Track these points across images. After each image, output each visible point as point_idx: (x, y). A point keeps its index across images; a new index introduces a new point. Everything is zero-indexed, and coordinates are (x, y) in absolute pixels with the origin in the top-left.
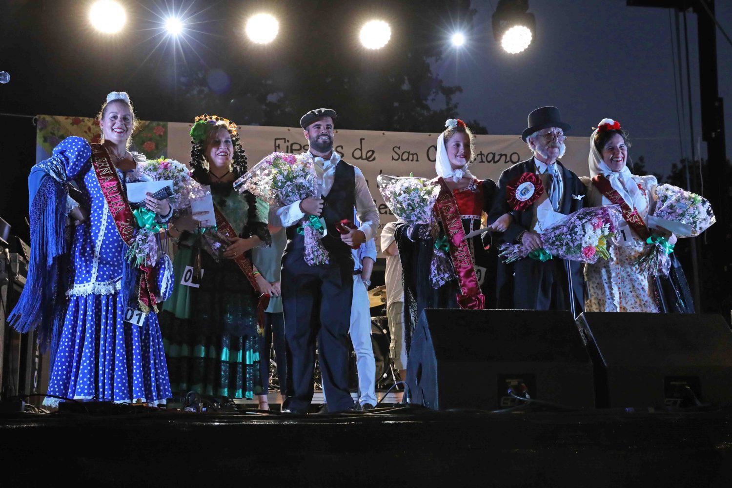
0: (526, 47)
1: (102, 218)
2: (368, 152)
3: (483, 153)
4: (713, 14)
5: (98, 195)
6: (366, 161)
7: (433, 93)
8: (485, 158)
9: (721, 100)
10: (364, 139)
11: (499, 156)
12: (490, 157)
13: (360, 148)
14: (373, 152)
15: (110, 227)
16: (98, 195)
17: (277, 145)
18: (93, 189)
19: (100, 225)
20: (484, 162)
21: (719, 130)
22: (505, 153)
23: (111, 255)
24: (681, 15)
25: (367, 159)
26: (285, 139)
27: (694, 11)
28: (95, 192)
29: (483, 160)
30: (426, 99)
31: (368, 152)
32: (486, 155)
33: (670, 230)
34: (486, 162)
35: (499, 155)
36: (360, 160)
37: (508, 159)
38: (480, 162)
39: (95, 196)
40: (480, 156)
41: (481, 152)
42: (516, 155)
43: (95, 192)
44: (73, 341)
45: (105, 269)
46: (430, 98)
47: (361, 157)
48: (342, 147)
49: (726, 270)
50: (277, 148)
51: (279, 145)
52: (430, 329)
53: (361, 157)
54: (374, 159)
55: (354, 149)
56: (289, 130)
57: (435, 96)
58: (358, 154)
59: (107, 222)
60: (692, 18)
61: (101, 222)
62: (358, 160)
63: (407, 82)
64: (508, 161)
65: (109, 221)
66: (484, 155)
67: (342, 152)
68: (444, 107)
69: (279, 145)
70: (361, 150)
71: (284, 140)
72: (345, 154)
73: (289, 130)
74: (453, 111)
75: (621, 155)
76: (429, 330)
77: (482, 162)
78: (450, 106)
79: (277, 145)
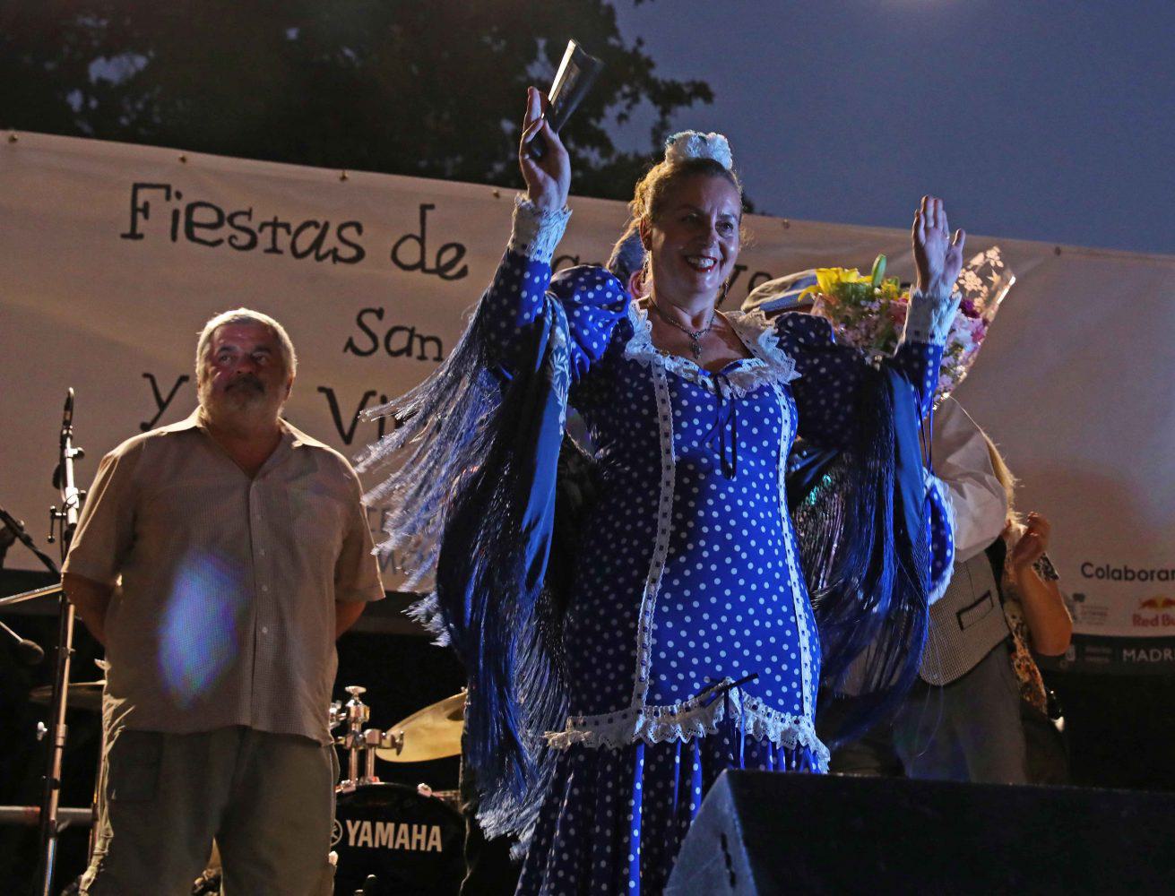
1: (656, 509)
2: (445, 248)
5: (644, 443)
6: (436, 277)
7: (625, 96)
8: (290, 238)
10: (432, 207)
13: (418, 234)
14: (461, 251)
15: (684, 535)
16: (644, 443)
17: (140, 205)
18: (628, 425)
19: (654, 533)
20: (280, 252)
22: (357, 220)
23: (688, 619)
25: (441, 271)
26: (168, 188)
28: (633, 433)
29: (279, 246)
31: (445, 248)
32: (293, 229)
36: (418, 272)
38: (124, 236)
39: (634, 446)
40: (268, 230)
43: (633, 433)
45: (674, 664)
46: (611, 112)
47: (421, 265)
50: (140, 216)
51: (146, 204)
52: (747, 844)
53: (421, 265)
54: (463, 273)
55: (398, 238)
56: (13, 140)
57: (629, 107)
58: (410, 253)
59: (674, 521)
61: (654, 524)
65: (679, 516)
69: (146, 204)
70: (421, 240)
71: (163, 192)
73: (787, 226)
75: (714, 252)
76: (744, 849)
77: (274, 250)
79: (140, 205)
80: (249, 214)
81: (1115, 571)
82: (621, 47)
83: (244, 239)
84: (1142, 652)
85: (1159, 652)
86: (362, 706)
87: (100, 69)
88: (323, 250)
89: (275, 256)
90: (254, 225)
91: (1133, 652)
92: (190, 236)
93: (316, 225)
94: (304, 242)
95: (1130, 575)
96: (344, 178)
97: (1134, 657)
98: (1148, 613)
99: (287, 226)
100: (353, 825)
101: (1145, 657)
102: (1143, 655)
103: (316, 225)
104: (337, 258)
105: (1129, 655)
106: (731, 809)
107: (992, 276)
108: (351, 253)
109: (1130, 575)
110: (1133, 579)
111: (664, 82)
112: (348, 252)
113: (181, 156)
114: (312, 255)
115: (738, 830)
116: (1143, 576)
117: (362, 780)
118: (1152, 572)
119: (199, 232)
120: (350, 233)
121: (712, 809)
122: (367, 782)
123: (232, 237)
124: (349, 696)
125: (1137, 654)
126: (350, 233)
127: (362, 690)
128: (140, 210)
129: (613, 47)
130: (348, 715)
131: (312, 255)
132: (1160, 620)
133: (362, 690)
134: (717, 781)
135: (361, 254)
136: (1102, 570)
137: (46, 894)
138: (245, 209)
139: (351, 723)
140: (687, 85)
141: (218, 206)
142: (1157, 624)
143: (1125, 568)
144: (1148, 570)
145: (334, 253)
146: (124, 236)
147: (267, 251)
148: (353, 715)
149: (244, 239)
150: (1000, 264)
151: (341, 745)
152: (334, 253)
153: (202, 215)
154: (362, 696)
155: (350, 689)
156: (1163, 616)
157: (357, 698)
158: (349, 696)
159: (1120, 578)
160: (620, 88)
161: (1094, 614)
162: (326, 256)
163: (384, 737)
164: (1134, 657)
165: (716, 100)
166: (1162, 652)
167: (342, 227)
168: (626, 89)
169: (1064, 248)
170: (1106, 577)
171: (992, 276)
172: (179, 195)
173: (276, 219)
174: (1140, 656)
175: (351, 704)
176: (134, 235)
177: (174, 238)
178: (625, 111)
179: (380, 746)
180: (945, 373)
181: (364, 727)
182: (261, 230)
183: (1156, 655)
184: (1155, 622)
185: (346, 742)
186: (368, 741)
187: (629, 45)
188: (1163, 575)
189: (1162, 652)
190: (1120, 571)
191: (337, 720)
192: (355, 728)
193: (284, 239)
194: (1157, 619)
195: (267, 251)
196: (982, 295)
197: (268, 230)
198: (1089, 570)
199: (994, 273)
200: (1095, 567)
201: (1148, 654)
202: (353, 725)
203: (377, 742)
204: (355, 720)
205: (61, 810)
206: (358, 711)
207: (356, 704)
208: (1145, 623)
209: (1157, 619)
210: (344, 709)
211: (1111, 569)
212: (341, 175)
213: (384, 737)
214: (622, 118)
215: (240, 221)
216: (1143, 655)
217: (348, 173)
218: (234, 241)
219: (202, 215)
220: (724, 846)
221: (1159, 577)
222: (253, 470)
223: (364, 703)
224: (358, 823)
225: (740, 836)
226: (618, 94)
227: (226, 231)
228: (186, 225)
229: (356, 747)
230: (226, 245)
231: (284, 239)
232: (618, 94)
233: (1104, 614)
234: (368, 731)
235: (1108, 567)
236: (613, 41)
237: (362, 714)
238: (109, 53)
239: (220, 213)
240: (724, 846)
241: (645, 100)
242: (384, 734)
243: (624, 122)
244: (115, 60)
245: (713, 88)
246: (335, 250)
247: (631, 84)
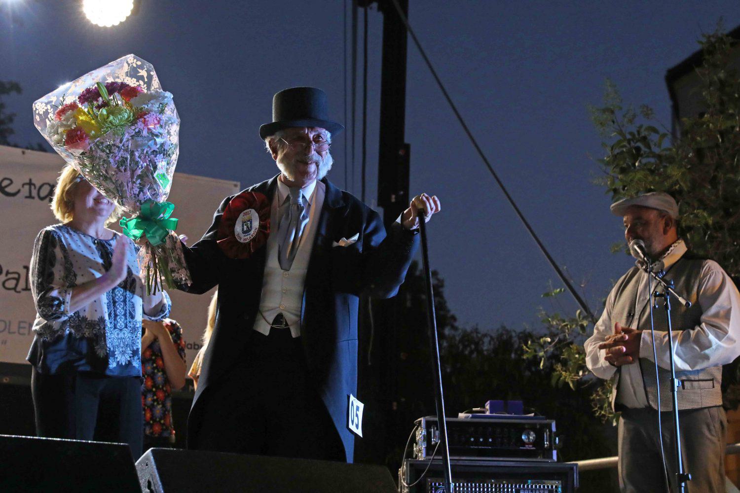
0: (123, 19)
2: (5, 179)
3: (33, 182)
4: (406, 12)
9: (407, 147)
12: (189, 346)
20: (33, 198)
21: (402, 193)
24: (361, 10)
27: (380, 8)
32: (38, 186)
34: (36, 198)
38: (27, 197)
40: (27, 187)
41: (30, 180)
47: (15, 289)
49: (395, 408)
60: (376, 18)
62: (8, 292)
66: (34, 185)
77: (30, 196)
107: (108, 80)
137: (683, 492)
143: (194, 343)
150: (139, 63)
159: (191, 348)
171: (108, 80)
190: (191, 345)
196: (49, 111)
199: (140, 70)
205: (37, 431)
211: (187, 343)
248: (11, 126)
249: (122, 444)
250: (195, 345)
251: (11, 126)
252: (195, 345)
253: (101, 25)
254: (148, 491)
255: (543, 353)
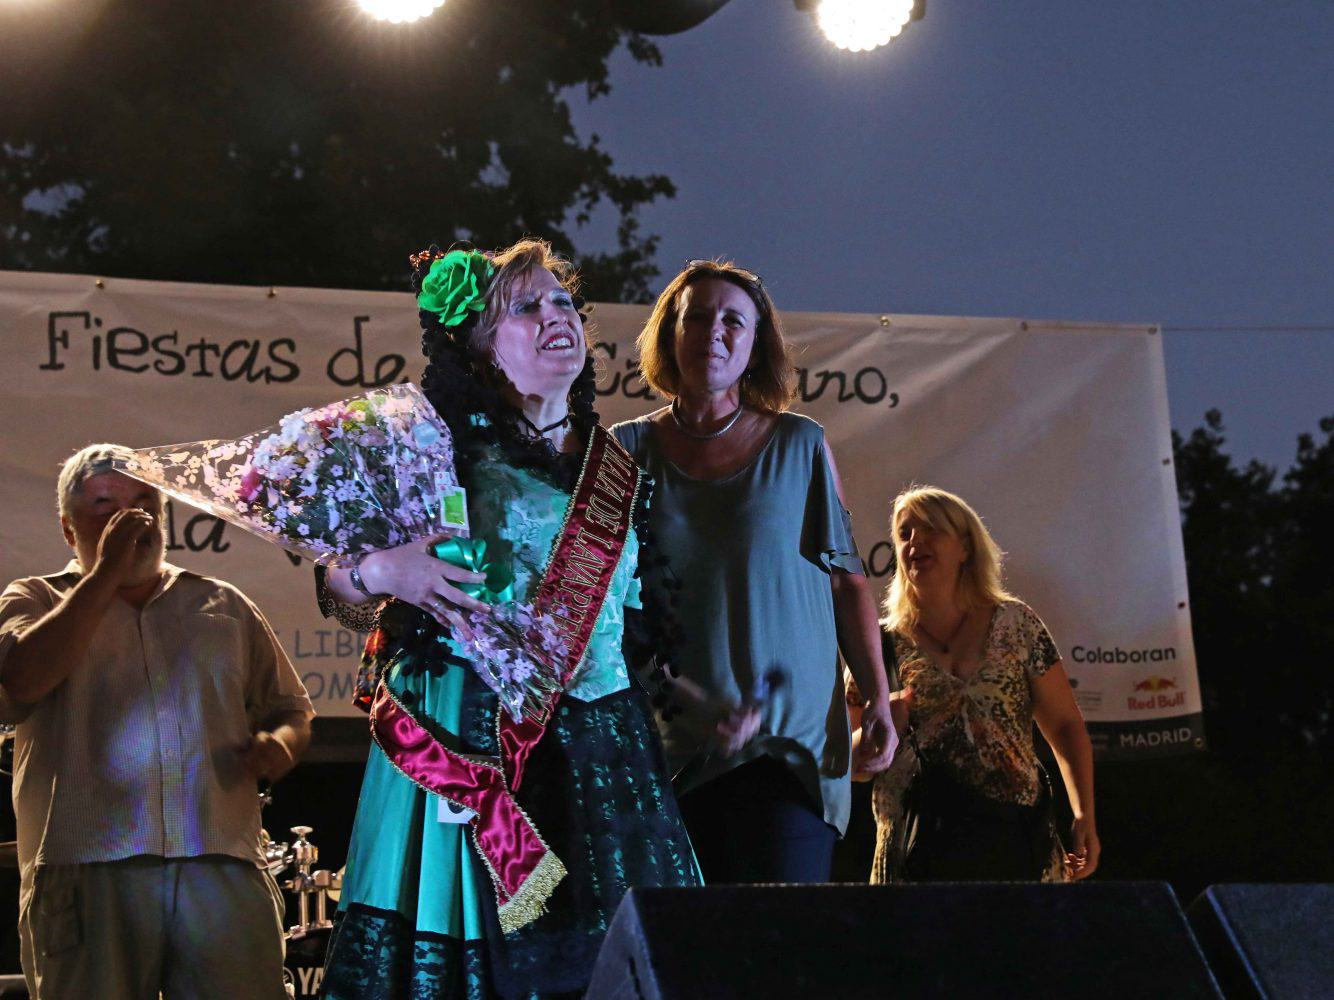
0: (896, 31)
7: (584, 196)
8: (218, 361)
10: (366, 319)
11: (820, 379)
13: (354, 347)
17: (58, 334)
20: (209, 375)
26: (86, 315)
30: (559, 218)
32: (222, 349)
33: (357, 708)
35: (818, 375)
37: (850, 388)
38: (43, 367)
40: (196, 353)
42: (874, 375)
44: (816, 592)
46: (571, 213)
48: (292, 346)
50: (59, 345)
51: (65, 334)
52: (655, 965)
55: (335, 351)
57: (588, 207)
63: (496, 160)
64: (850, 396)
67: (293, 361)
68: (614, 250)
70: (358, 354)
71: (82, 320)
72: (303, 371)
74: (642, 264)
77: (203, 372)
78: (633, 245)
79: (58, 334)
80: (174, 337)
81: (1106, 653)
82: (576, 146)
83: (170, 363)
84: (1140, 736)
85: (1157, 735)
86: (309, 846)
87: (37, 201)
88: (255, 370)
89: (204, 379)
90: (181, 349)
91: (1131, 737)
92: (114, 362)
93: (245, 344)
94: (233, 365)
95: (1122, 657)
96: (271, 295)
97: (1132, 743)
98: (1144, 696)
99: (215, 348)
100: (305, 972)
101: (1143, 741)
102: (1141, 739)
103: (245, 344)
104: (270, 378)
105: (1127, 740)
106: (637, 929)
108: (284, 371)
109: (1122, 657)
110: (1125, 661)
111: (623, 179)
112: (281, 371)
113: (98, 282)
114: (245, 375)
115: (645, 951)
116: (1135, 657)
117: (313, 925)
118: (1145, 653)
119: (122, 359)
120: (282, 351)
121: (621, 931)
122: (318, 926)
123: (157, 363)
124: (294, 838)
125: (1135, 740)
126: (282, 351)
127: (308, 829)
128: (57, 339)
129: (568, 146)
130: (295, 857)
131: (244, 376)
132: (1156, 701)
133: (308, 829)
134: (623, 902)
135: (295, 372)
136: (1093, 653)
138: (170, 332)
139: (299, 866)
140: (648, 180)
141: (142, 331)
142: (1153, 707)
143: (1117, 649)
144: (1162, 647)
145: (267, 373)
146: (43, 367)
147: (196, 374)
148: (299, 856)
149: (170, 363)
151: (290, 889)
152: (267, 373)
153: (121, 341)
154: (309, 837)
155: (295, 829)
156: (1159, 698)
157: (304, 839)
158: (294, 838)
159: (1112, 661)
160: (577, 188)
161: (1089, 699)
162: (258, 376)
163: (335, 878)
164: (1132, 743)
165: (678, 194)
166: (1161, 734)
167: (273, 345)
168: (585, 188)
169: (1031, 323)
170: (1097, 659)
172: (98, 322)
173: (203, 340)
174: (1138, 741)
175: (297, 845)
176: (53, 365)
177: (97, 365)
178: (584, 211)
179: (330, 887)
180: (373, 418)
181: (313, 868)
182: (188, 353)
183: (1154, 739)
184: (1150, 705)
185: (294, 886)
186: (317, 883)
187: (585, 143)
188: (1156, 655)
189: (1161, 734)
190: (1111, 654)
191: (284, 863)
192: (304, 870)
193: (213, 362)
194: (1153, 700)
195: (196, 374)
197: (196, 353)
198: (1079, 654)
200: (1086, 651)
201: (1146, 738)
202: (301, 867)
203: (326, 883)
204: (303, 861)
206: (305, 850)
207: (303, 844)
208: (1141, 706)
209: (1153, 700)
210: (291, 851)
211: (1102, 652)
212: (268, 293)
213: (335, 878)
214: (582, 218)
215: (164, 345)
216: (1141, 739)
217: (276, 290)
218: (160, 366)
219: (121, 341)
220: (633, 970)
221: (1152, 658)
222: (138, 605)
223: (312, 843)
224: (310, 970)
225: (648, 958)
226: (577, 195)
227: (151, 356)
228: (107, 351)
229: (305, 890)
230: (152, 370)
231: (213, 362)
232: (577, 195)
233: (1099, 699)
234: (317, 873)
235: (1099, 650)
236: (568, 140)
237: (310, 855)
238: (44, 185)
239: (143, 337)
240: (633, 970)
241: (605, 199)
242: (334, 875)
243: (584, 223)
244: (50, 192)
245: (674, 181)
246: (267, 370)
247: (589, 184)
248: (653, 260)
249: (796, 884)
250: (1118, 653)
251: (653, 260)
252: (1118, 653)
253: (855, 48)
254: (637, 997)
255: (176, 571)
